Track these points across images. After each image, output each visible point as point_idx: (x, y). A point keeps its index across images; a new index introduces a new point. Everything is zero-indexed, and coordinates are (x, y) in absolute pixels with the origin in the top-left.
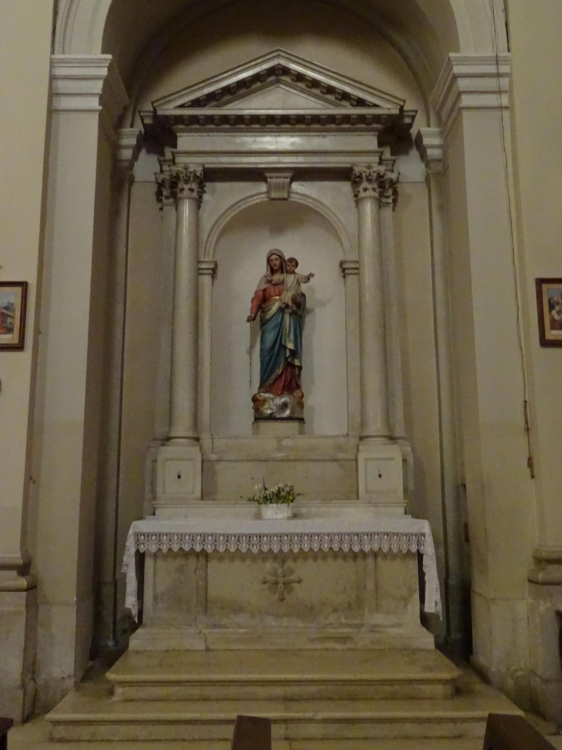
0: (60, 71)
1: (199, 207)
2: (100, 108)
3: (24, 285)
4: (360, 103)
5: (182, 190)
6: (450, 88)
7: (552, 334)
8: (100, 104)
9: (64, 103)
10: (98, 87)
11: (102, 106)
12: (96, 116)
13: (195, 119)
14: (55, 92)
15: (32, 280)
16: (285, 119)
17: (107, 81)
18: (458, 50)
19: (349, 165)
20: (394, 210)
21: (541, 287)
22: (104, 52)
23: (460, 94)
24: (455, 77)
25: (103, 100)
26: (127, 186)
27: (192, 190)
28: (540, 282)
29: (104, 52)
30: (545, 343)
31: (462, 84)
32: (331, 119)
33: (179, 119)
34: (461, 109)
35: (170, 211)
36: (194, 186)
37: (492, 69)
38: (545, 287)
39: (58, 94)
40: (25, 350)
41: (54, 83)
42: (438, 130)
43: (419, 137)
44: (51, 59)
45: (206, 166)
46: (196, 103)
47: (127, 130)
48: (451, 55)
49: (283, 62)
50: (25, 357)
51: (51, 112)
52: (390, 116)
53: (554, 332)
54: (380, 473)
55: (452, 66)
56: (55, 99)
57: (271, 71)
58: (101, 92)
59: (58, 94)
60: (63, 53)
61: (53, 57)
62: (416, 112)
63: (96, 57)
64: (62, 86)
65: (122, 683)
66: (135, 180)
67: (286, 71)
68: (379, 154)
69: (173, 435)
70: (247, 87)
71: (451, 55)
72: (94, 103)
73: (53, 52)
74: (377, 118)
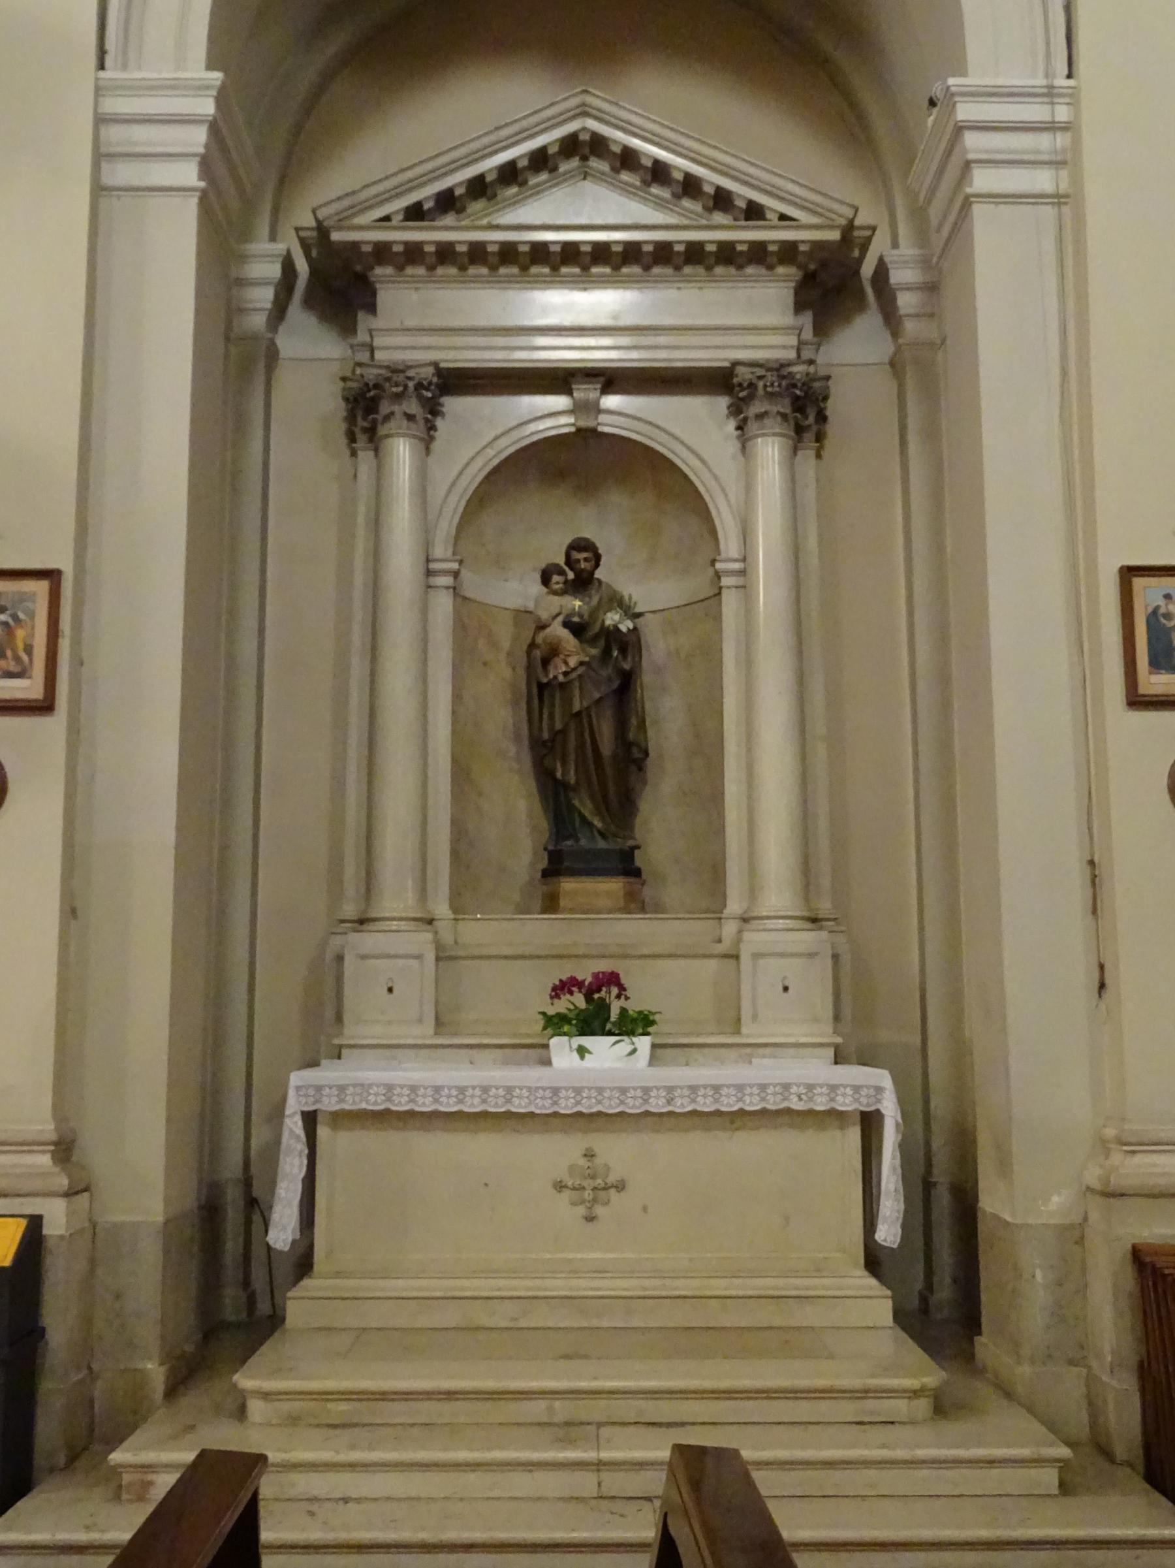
0: (115, 105)
1: (428, 450)
2: (202, 184)
3: (52, 576)
4: (754, 212)
5: (388, 417)
6: (949, 153)
7: (1156, 683)
8: (200, 178)
9: (121, 174)
10: (198, 137)
11: (204, 180)
12: (193, 202)
13: (413, 254)
14: (103, 150)
15: (63, 561)
16: (601, 253)
17: (214, 128)
18: (964, 74)
19: (726, 364)
20: (819, 456)
21: (1130, 583)
22: (210, 67)
23: (967, 165)
24: (960, 129)
25: (206, 166)
26: (261, 366)
27: (410, 418)
28: (1129, 573)
29: (210, 67)
30: (1137, 701)
31: (972, 140)
32: (695, 254)
33: (382, 252)
34: (968, 197)
35: (366, 457)
36: (413, 407)
37: (1036, 112)
38: (1139, 583)
39: (111, 156)
40: (56, 712)
41: (103, 130)
42: (917, 252)
43: (882, 271)
44: (97, 79)
45: (443, 365)
46: (415, 213)
47: (261, 245)
48: (951, 81)
49: (592, 124)
50: (54, 726)
51: (99, 190)
52: (818, 245)
53: (1155, 678)
54: (787, 984)
55: (955, 102)
56: (105, 166)
57: (571, 146)
58: (202, 150)
59: (111, 156)
60: (125, 67)
61: (102, 74)
62: (874, 229)
63: (195, 75)
64: (114, 134)
65: (266, 1396)
66: (281, 356)
67: (598, 145)
68: (797, 332)
69: (373, 915)
70: (522, 184)
71: (951, 81)
72: (188, 174)
73: (102, 66)
74: (788, 252)
